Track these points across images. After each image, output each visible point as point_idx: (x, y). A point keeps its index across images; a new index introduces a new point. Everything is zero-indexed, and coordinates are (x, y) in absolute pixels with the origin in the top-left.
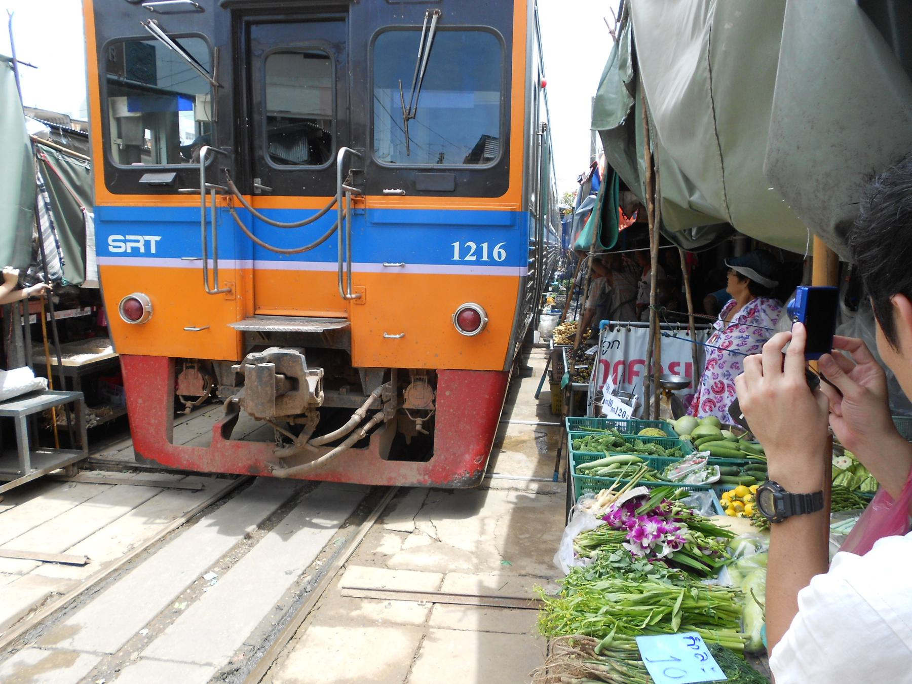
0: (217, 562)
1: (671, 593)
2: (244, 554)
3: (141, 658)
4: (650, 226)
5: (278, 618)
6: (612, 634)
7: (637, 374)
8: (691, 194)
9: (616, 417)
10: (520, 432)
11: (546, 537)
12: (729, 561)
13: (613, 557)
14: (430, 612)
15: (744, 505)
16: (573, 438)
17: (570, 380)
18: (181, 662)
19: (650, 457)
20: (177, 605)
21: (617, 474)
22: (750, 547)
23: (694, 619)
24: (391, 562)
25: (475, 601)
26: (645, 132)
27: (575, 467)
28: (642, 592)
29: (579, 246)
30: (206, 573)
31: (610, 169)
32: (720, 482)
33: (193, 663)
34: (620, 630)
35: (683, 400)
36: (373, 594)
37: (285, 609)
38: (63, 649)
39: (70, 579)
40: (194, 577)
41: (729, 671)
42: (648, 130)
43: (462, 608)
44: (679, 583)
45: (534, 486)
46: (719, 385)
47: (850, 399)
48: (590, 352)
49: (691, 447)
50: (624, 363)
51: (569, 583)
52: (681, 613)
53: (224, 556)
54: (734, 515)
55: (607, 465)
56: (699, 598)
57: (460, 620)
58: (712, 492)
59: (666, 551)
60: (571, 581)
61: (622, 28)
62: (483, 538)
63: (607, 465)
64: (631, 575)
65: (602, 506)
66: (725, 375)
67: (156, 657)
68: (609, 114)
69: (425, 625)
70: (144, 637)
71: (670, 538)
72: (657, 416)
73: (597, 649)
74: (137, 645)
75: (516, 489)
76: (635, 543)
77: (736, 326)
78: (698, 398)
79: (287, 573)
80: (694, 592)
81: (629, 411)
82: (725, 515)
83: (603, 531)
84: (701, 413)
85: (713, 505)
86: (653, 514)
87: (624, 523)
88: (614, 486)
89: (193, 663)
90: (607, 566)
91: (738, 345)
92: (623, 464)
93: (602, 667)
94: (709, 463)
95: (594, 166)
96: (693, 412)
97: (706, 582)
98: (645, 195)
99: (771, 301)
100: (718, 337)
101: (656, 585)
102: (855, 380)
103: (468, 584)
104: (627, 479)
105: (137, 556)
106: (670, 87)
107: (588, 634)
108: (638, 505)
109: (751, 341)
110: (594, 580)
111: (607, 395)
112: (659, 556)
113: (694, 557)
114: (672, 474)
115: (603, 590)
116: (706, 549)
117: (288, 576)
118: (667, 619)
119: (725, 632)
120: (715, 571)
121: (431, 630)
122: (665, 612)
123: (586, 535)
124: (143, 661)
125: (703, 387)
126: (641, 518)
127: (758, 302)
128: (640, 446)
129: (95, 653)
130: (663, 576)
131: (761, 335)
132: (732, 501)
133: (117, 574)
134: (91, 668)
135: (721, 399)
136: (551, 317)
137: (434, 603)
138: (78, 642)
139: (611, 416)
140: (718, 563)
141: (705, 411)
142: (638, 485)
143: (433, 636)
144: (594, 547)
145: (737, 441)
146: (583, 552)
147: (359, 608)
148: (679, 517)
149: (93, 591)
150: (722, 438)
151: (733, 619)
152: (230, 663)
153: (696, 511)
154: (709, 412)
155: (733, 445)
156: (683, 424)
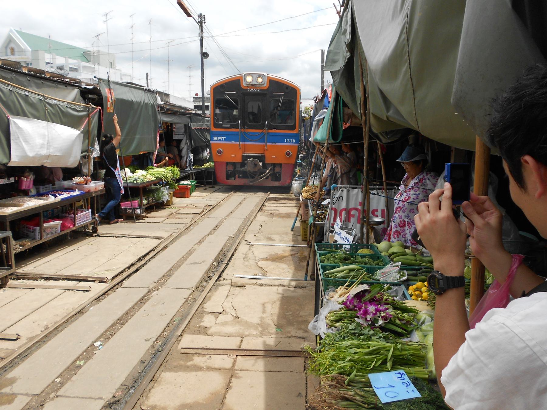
0: (102, 335)
1: (386, 347)
2: (119, 329)
3: (57, 396)
4: (364, 129)
5: (142, 368)
6: (354, 373)
7: (353, 216)
8: (388, 109)
9: (343, 242)
10: (283, 251)
11: (302, 313)
12: (416, 327)
13: (351, 327)
14: (235, 360)
15: (422, 293)
16: (320, 255)
17: (314, 220)
18: (83, 398)
19: (366, 266)
20: (78, 362)
21: (348, 277)
22: (428, 318)
23: (400, 362)
24: (209, 332)
25: (262, 353)
26: (360, 73)
27: (323, 273)
28: (369, 347)
29: (316, 139)
30: (95, 342)
31: (337, 95)
32: (407, 280)
33: (91, 398)
34: (358, 371)
35: (380, 232)
36: (200, 351)
37: (146, 363)
38: (6, 393)
39: (7, 349)
40: (88, 345)
41: (422, 392)
42: (362, 72)
43: (254, 358)
44: (389, 341)
45: (293, 283)
46: (403, 222)
47: (478, 227)
48: (325, 203)
49: (389, 259)
50: (345, 210)
51: (326, 343)
52: (392, 359)
53: (106, 331)
54: (417, 300)
55: (342, 271)
56: (402, 350)
57: (253, 365)
58: (403, 286)
59: (381, 322)
60: (327, 342)
61: (344, 10)
62: (264, 315)
63: (342, 271)
64: (362, 337)
65: (340, 296)
66: (406, 216)
67: (67, 395)
68: (335, 62)
69: (232, 369)
70: (58, 383)
71: (383, 315)
72: (368, 242)
73: (346, 382)
74: (54, 389)
75: (283, 286)
76: (362, 318)
77: (413, 188)
78: (391, 230)
79: (146, 341)
80: (399, 346)
81: (351, 238)
82: (411, 299)
83: (343, 311)
84: (392, 239)
85: (404, 294)
86: (373, 301)
87: (355, 306)
88: (347, 284)
89: (91, 398)
90: (348, 332)
91: (413, 199)
92: (351, 270)
93: (350, 393)
94: (401, 269)
95: (324, 92)
96: (387, 238)
97: (405, 340)
98: (359, 111)
99: (432, 174)
100: (402, 194)
101: (377, 343)
102: (483, 218)
103: (256, 343)
104: (354, 280)
105: (51, 333)
106: (379, 47)
107: (340, 373)
108: (364, 296)
109: (421, 197)
110: (340, 341)
111: (337, 229)
112: (377, 325)
113: (396, 325)
114: (378, 275)
115: (347, 347)
116: (403, 320)
117: (147, 342)
118: (385, 362)
119: (417, 369)
120: (409, 333)
121: (236, 372)
122: (384, 358)
123: (332, 314)
124: (59, 398)
125: (393, 224)
126: (365, 303)
127: (425, 174)
128: (359, 259)
129: (27, 395)
130: (380, 337)
131: (426, 193)
132: (414, 291)
133: (38, 344)
134: (25, 404)
135: (404, 231)
136: (299, 182)
137: (237, 356)
138: (16, 388)
139: (340, 242)
140: (410, 328)
141: (395, 238)
142: (362, 283)
143: (237, 375)
144: (337, 321)
145: (415, 256)
146: (331, 324)
147: (192, 360)
148: (387, 302)
149: (23, 356)
150: (406, 255)
151: (421, 361)
152: (114, 397)
153: (395, 298)
154: (397, 238)
155: (413, 258)
156: (383, 245)
